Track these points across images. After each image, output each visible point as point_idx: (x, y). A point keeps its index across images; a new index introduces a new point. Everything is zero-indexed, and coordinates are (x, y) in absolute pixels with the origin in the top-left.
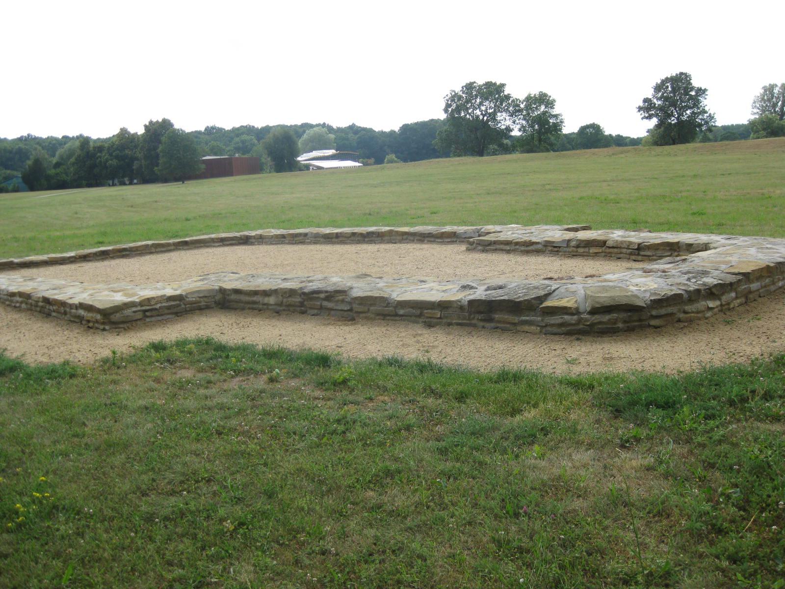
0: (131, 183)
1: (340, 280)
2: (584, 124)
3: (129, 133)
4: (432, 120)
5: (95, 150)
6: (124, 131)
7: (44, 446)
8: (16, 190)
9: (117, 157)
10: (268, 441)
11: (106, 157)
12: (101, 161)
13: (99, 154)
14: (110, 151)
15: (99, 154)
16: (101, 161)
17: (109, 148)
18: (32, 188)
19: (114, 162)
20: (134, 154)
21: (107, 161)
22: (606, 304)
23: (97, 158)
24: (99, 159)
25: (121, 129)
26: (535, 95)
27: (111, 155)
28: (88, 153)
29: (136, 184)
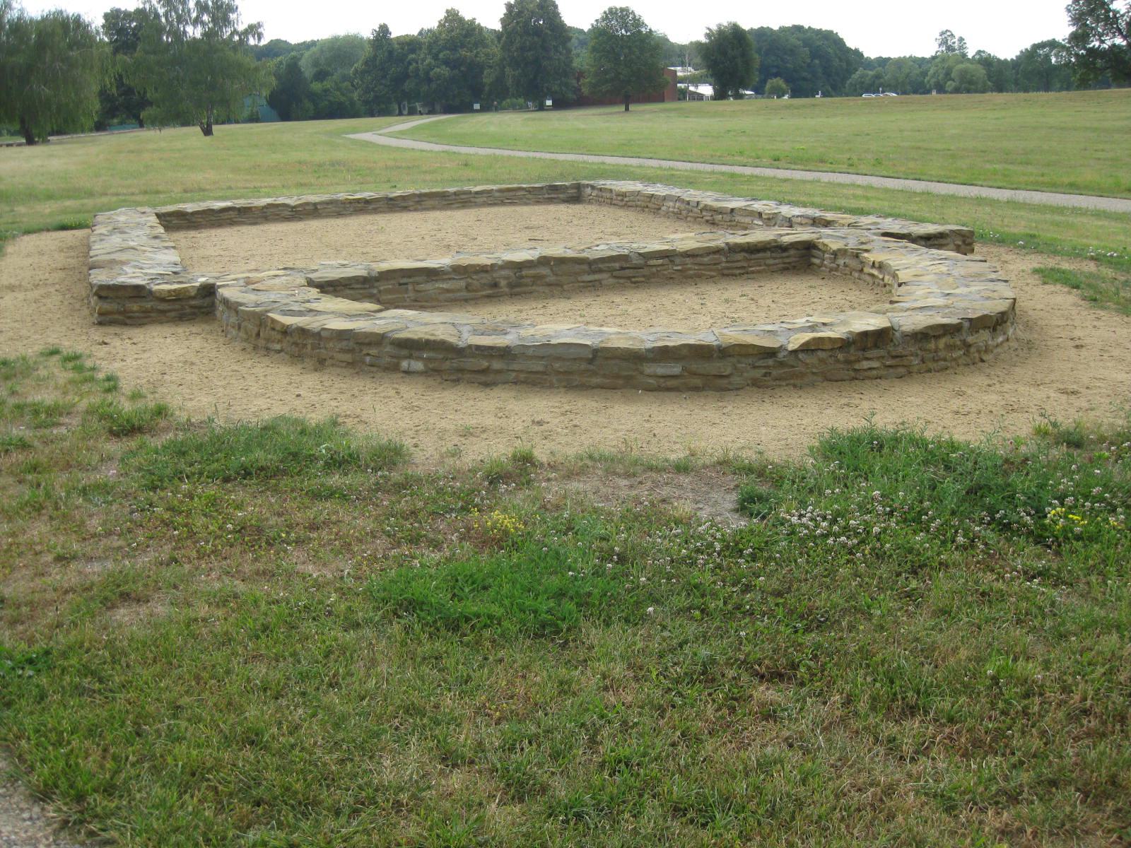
0: (400, 114)
1: (422, 287)
2: (1038, 41)
3: (461, 20)
4: (798, 29)
5: (403, 49)
6: (452, 17)
7: (1114, 783)
8: (254, 119)
9: (446, 62)
10: (100, 621)
11: (427, 62)
12: (417, 69)
13: (412, 56)
14: (434, 51)
15: (412, 56)
16: (417, 69)
17: (430, 46)
18: (285, 116)
19: (444, 71)
20: (476, 56)
21: (431, 68)
22: (438, 311)
23: (410, 63)
24: (414, 64)
25: (447, 11)
26: (254, 29)
27: (436, 57)
28: (391, 53)
29: (477, 111)
